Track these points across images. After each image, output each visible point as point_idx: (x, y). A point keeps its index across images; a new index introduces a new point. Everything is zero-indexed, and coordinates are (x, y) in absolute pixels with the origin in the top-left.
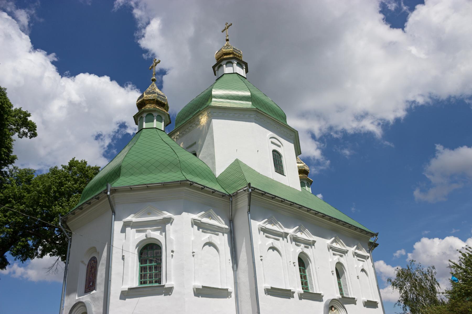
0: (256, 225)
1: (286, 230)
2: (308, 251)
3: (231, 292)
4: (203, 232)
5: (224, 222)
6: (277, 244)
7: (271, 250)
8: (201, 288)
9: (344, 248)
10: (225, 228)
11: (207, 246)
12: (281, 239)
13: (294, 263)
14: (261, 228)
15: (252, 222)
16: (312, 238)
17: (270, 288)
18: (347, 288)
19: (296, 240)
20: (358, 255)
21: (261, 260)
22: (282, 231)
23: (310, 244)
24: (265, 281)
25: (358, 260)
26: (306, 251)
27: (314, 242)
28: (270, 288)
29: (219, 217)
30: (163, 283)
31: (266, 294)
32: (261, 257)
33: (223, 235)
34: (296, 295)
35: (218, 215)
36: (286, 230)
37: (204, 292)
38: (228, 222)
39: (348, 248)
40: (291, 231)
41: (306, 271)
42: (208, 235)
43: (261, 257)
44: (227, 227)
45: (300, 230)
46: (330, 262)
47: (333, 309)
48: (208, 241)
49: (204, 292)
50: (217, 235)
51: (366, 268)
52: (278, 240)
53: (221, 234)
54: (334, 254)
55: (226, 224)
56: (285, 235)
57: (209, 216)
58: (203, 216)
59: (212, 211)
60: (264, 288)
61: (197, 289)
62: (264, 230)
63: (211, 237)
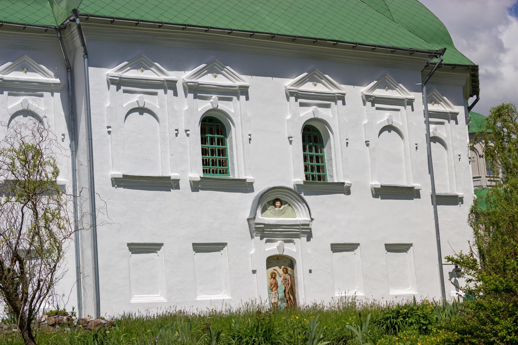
0: (98, 77)
1: (172, 75)
2: (231, 108)
3: (63, 186)
4: (9, 94)
5: (52, 74)
6: (149, 101)
7: (137, 113)
8: (199, 179)
9: (335, 91)
10: (55, 84)
11: (20, 119)
12: (161, 92)
13: (186, 131)
14: (110, 79)
15: (89, 68)
16: (245, 80)
17: (122, 177)
18: (331, 165)
19: (196, 91)
20: (374, 100)
21: (109, 132)
22: (162, 77)
23: (227, 93)
24: (113, 166)
25: (377, 109)
26: (223, 106)
27: (244, 91)
28: (122, 177)
29: (43, 66)
30: (329, 180)
31: (113, 186)
32: (109, 127)
33: (52, 95)
34: (185, 185)
35: (39, 64)
36: (172, 75)
37: (385, 192)
38: (63, 71)
39: (345, 89)
40: (183, 77)
41: (228, 140)
42: (21, 99)
43: (109, 127)
44: (58, 81)
45: (312, 78)
46: (288, 120)
47: (278, 203)
48: (21, 108)
49: (385, 192)
50: (42, 96)
51: (397, 123)
52: (155, 94)
53: (47, 94)
54: (302, 105)
55: (56, 76)
56: (171, 85)
57: (25, 68)
58: (9, 70)
59: (28, 59)
60: (110, 177)
61: (194, 182)
62: (118, 83)
63: (25, 101)
